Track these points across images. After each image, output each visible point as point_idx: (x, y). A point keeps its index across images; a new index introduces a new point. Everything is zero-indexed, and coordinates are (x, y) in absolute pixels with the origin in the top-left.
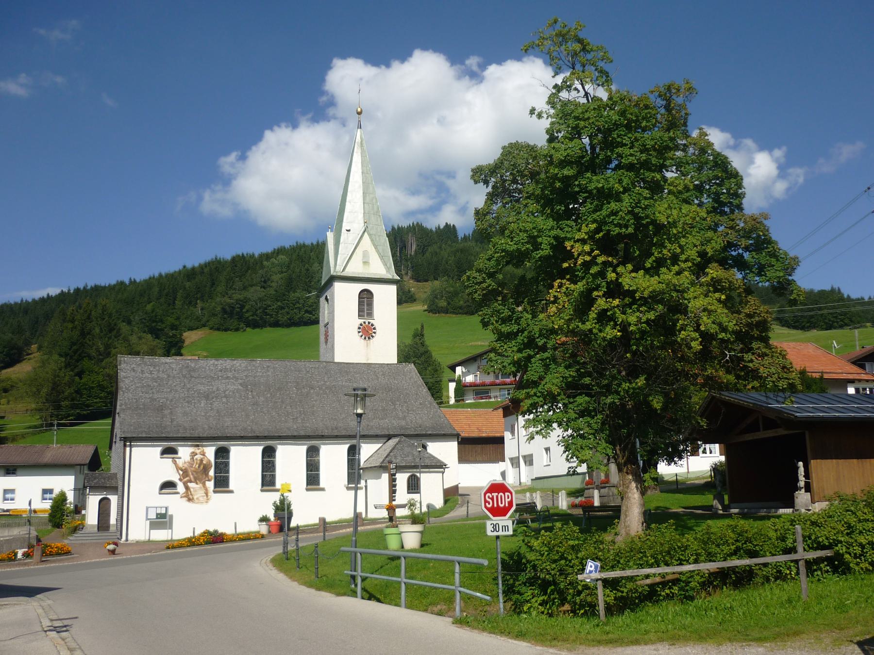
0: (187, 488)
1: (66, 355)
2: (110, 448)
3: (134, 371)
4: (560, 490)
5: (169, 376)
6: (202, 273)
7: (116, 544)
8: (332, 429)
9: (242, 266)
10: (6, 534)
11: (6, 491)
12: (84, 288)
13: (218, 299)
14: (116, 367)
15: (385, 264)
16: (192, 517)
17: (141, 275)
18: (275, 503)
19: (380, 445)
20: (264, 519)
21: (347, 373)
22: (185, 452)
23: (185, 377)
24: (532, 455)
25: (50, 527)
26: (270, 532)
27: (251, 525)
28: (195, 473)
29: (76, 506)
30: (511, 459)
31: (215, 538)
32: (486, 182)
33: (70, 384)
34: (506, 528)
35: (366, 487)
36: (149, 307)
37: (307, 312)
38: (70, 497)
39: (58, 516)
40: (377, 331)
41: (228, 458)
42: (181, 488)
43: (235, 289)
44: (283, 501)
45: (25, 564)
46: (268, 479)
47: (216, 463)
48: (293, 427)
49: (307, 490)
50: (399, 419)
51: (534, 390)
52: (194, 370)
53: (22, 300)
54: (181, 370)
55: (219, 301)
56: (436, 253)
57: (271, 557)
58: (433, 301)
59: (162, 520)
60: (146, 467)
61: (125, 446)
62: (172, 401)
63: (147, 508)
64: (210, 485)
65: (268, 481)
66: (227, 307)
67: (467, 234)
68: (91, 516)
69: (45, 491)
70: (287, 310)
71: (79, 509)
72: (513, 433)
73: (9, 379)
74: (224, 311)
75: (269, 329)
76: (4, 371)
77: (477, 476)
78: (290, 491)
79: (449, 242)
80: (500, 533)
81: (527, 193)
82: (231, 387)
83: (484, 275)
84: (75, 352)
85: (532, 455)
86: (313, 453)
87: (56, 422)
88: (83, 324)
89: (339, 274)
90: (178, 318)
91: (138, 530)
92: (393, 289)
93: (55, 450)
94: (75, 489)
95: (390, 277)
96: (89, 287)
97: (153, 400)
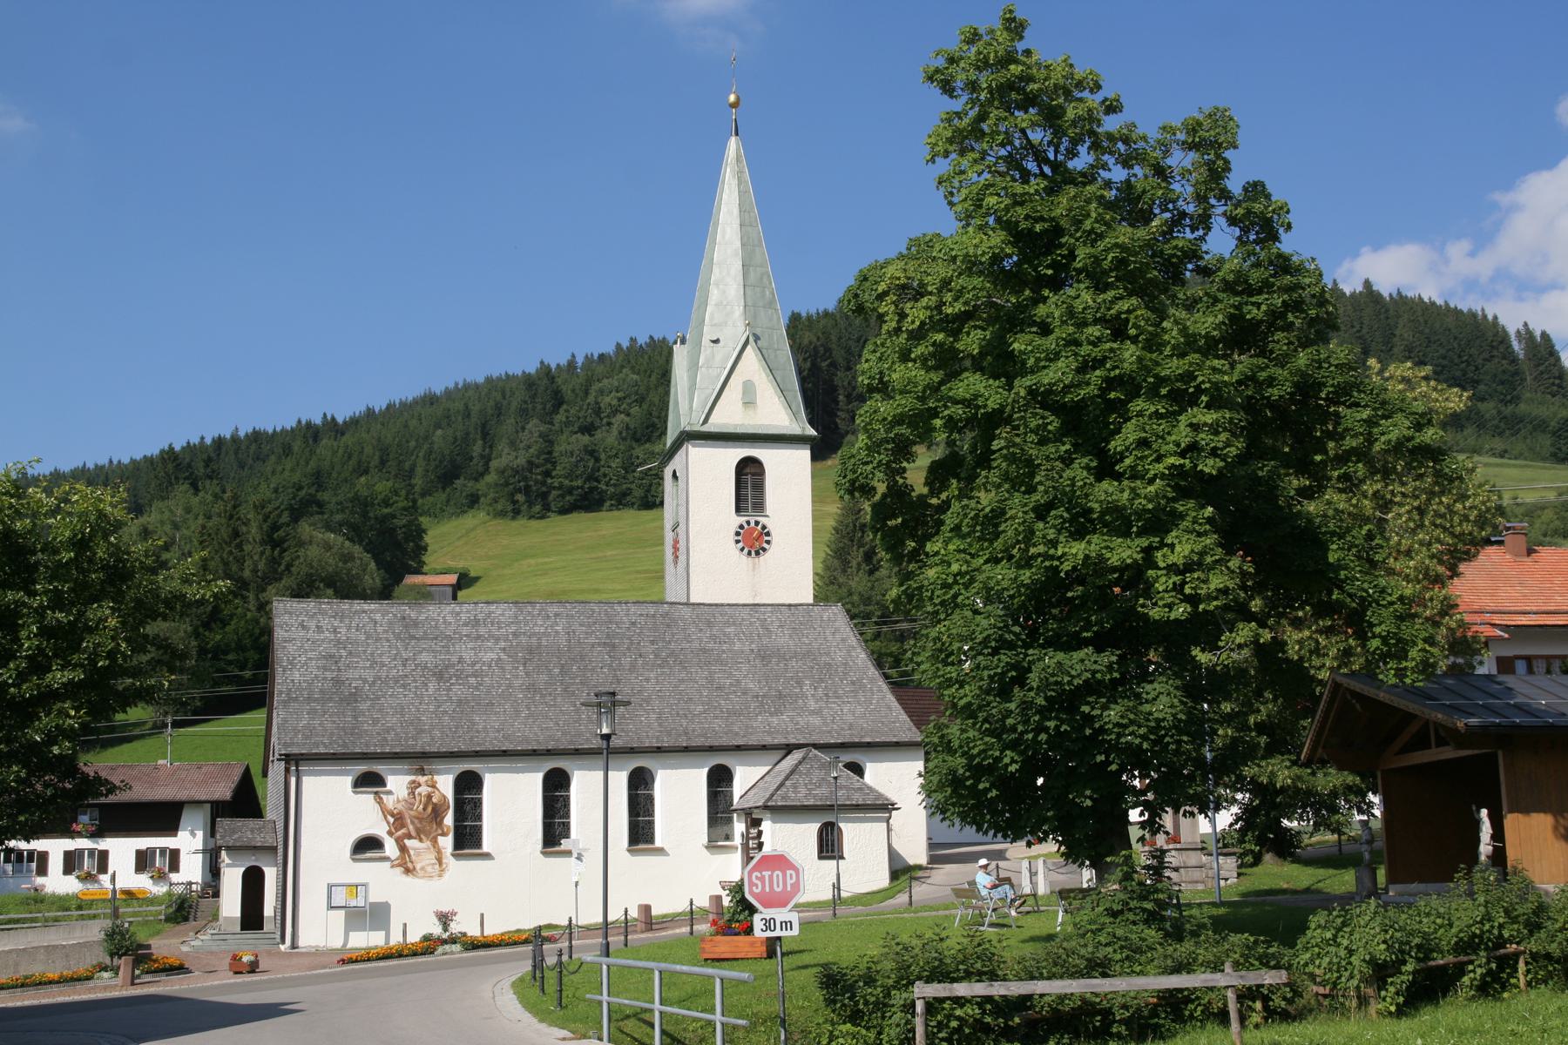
0: (403, 849)
3: (304, 627)
19: (767, 768)
22: (398, 783)
34: (787, 925)
40: (775, 538)
42: (391, 848)
49: (820, 858)
52: (416, 624)
54: (390, 623)
57: (514, 978)
60: (330, 810)
63: (330, 887)
64: (447, 842)
68: (231, 902)
80: (777, 933)
87: (169, 720)
96: (242, 434)
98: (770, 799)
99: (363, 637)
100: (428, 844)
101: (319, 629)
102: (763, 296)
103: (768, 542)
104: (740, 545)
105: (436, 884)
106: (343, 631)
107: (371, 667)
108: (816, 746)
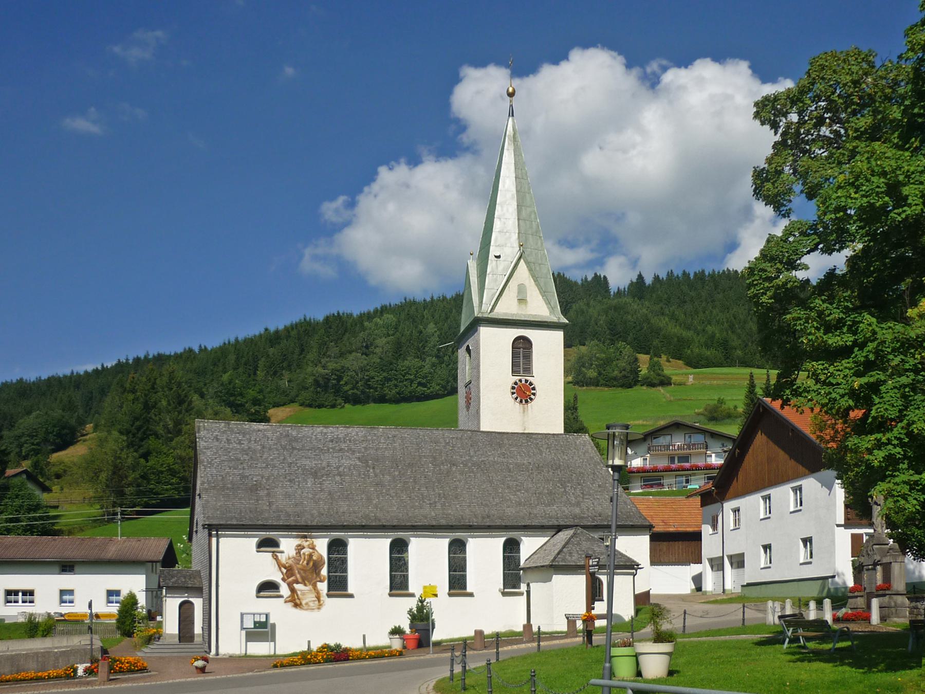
0: (293, 590)
1: (128, 432)
2: (190, 539)
3: (217, 440)
4: (787, 598)
5: (263, 447)
6: (288, 337)
7: (206, 660)
8: (483, 518)
9: (338, 326)
10: (64, 643)
11: (63, 592)
12: (145, 357)
13: (309, 369)
14: (194, 434)
15: (548, 302)
16: (301, 628)
17: (213, 342)
18: (411, 610)
19: (547, 539)
20: (397, 631)
21: (500, 446)
22: (288, 545)
23: (284, 448)
24: (743, 554)
25: (118, 636)
26: (404, 647)
27: (380, 639)
28: (301, 572)
29: (149, 612)
30: (711, 561)
31: (338, 655)
32: (775, 126)
33: (134, 468)
35: (528, 592)
36: (225, 377)
37: (420, 384)
38: (142, 600)
39: (128, 623)
41: (345, 553)
42: (284, 590)
43: (329, 356)
44: (421, 608)
45: (88, 683)
46: (398, 580)
47: (329, 559)
48: (429, 514)
50: (572, 505)
51: (888, 435)
52: (296, 440)
53: (72, 373)
54: (279, 439)
55: (312, 371)
56: (583, 312)
58: (580, 370)
59: (262, 630)
60: (239, 563)
61: (210, 535)
62: (268, 479)
63: (242, 615)
64: (323, 587)
65: (398, 583)
66: (320, 379)
67: (622, 288)
68: (171, 624)
69: (110, 593)
70: (394, 382)
71: (154, 613)
72: (714, 527)
73: (61, 463)
74: (317, 383)
75: (372, 405)
76: (55, 455)
77: (670, 581)
78: (436, 595)
79: (599, 298)
81: (856, 130)
82: (346, 463)
83: (778, 265)
84: (139, 429)
85: (743, 554)
86: (457, 548)
88: (146, 395)
89: (486, 315)
90: (261, 391)
91: (231, 642)
92: (559, 335)
93: (119, 541)
94: (147, 590)
95: (555, 319)
96: (151, 356)
97: (243, 477)
98: (553, 561)
99: (259, 447)
100: (310, 587)
101: (228, 441)
102: (531, 227)
103: (534, 394)
104: (515, 396)
105: (316, 614)
106: (246, 443)
107: (267, 467)
108: (584, 527)
